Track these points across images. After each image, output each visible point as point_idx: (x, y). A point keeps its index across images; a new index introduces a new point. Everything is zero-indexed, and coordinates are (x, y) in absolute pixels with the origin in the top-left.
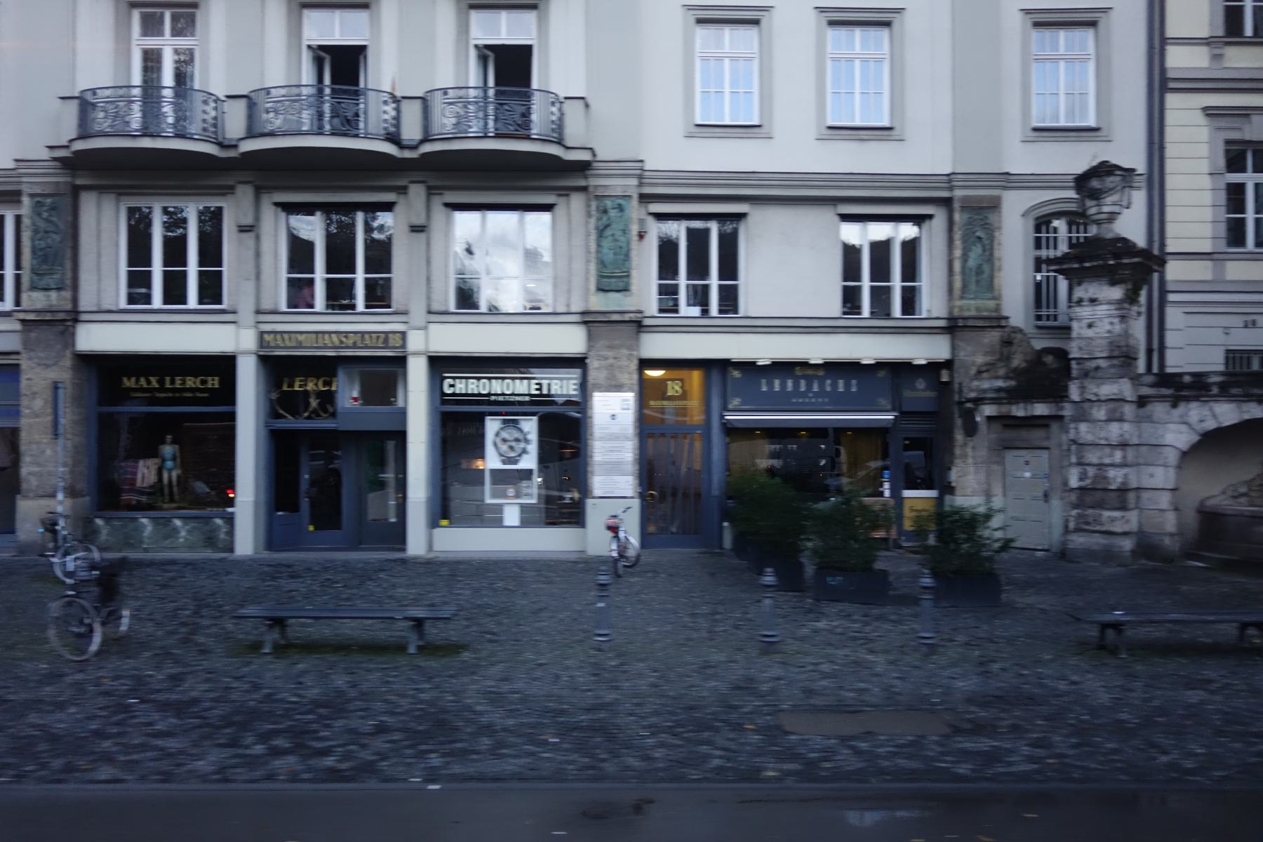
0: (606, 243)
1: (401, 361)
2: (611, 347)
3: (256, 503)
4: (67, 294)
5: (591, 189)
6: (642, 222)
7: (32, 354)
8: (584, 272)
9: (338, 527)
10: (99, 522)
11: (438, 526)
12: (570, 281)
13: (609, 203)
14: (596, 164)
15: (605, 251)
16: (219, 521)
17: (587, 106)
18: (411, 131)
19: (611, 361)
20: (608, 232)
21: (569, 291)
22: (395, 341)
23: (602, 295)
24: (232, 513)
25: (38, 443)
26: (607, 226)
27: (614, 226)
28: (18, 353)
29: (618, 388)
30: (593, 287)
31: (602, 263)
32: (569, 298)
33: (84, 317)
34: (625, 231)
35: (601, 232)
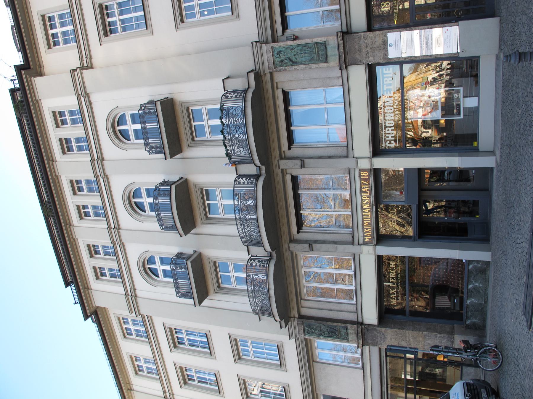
0: (299, 59)
1: (377, 172)
2: (360, 51)
3: (460, 249)
4: (349, 326)
5: (271, 71)
6: (288, 39)
7: (379, 343)
8: (318, 70)
9: (478, 201)
10: (468, 322)
11: (477, 147)
12: (324, 78)
13: (277, 60)
14: (257, 70)
15: (304, 59)
16: (471, 267)
17: (228, 78)
18: (250, 169)
19: (368, 49)
20: (293, 58)
21: (330, 78)
22: (365, 174)
23: (329, 59)
24: (466, 260)
25: (424, 345)
26: (291, 60)
27: (289, 56)
28: (380, 349)
29: (385, 43)
30: (325, 65)
31: (311, 61)
32: (334, 78)
33: (360, 320)
34: (292, 48)
35: (294, 63)
